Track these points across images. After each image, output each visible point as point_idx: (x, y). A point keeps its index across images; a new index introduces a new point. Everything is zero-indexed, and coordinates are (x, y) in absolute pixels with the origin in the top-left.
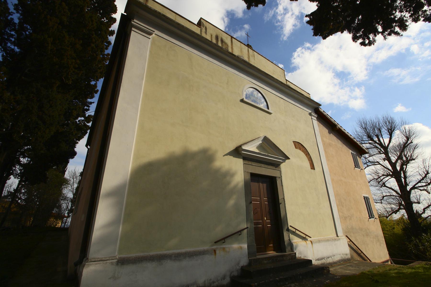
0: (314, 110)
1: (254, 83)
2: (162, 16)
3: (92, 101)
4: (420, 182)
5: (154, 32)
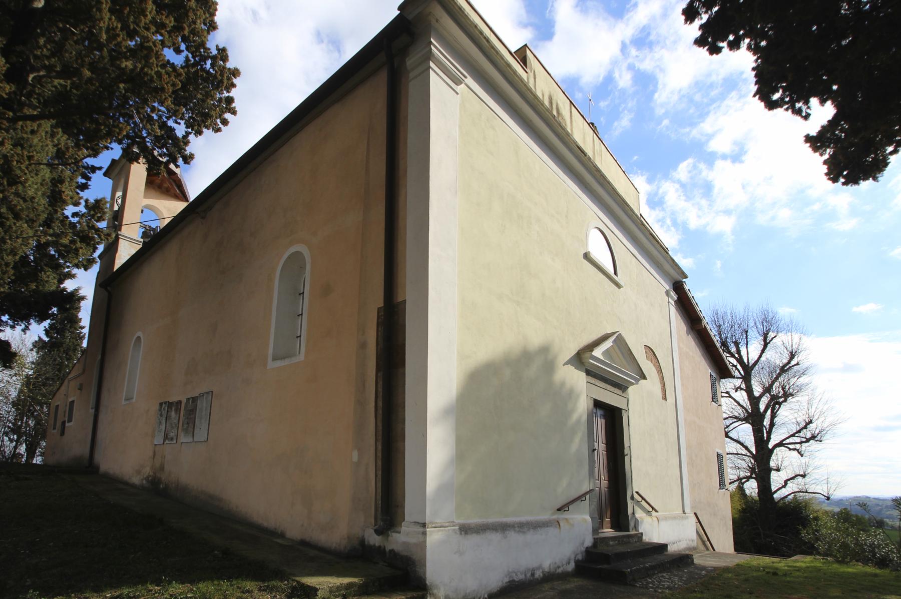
0: (673, 284)
1: (600, 219)
2: (483, 39)
3: (97, 165)
4: (793, 435)
5: (466, 77)
